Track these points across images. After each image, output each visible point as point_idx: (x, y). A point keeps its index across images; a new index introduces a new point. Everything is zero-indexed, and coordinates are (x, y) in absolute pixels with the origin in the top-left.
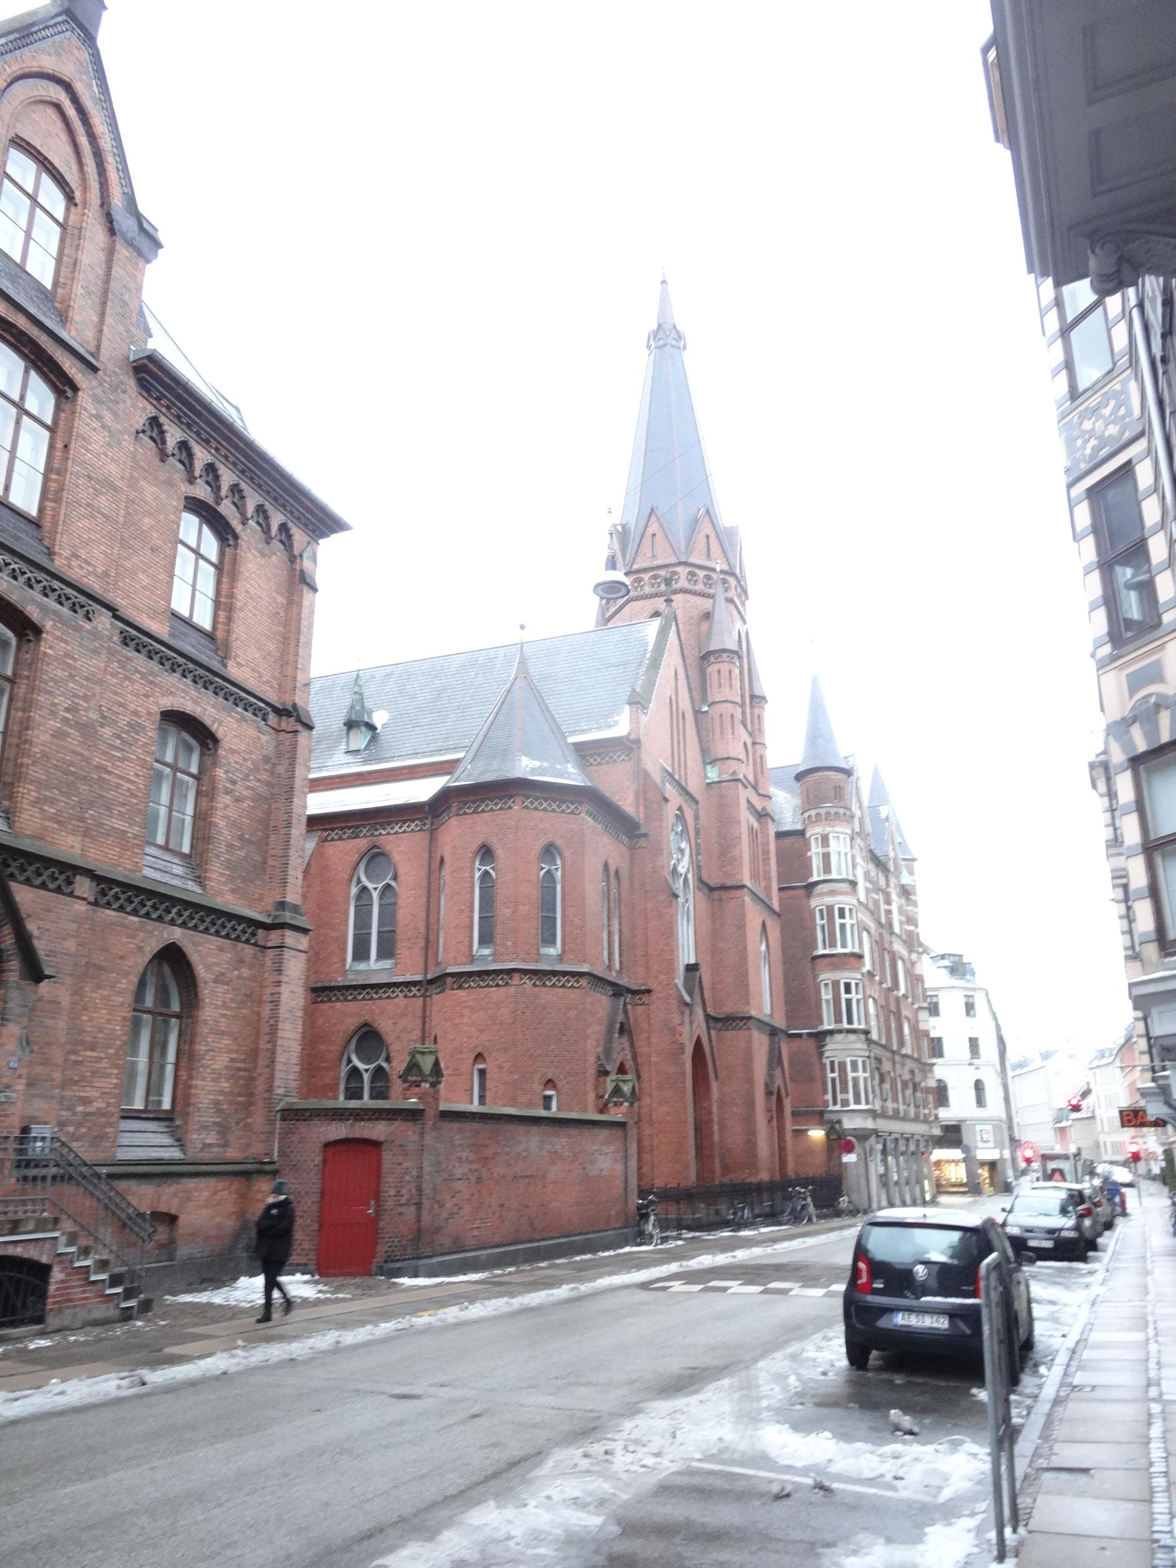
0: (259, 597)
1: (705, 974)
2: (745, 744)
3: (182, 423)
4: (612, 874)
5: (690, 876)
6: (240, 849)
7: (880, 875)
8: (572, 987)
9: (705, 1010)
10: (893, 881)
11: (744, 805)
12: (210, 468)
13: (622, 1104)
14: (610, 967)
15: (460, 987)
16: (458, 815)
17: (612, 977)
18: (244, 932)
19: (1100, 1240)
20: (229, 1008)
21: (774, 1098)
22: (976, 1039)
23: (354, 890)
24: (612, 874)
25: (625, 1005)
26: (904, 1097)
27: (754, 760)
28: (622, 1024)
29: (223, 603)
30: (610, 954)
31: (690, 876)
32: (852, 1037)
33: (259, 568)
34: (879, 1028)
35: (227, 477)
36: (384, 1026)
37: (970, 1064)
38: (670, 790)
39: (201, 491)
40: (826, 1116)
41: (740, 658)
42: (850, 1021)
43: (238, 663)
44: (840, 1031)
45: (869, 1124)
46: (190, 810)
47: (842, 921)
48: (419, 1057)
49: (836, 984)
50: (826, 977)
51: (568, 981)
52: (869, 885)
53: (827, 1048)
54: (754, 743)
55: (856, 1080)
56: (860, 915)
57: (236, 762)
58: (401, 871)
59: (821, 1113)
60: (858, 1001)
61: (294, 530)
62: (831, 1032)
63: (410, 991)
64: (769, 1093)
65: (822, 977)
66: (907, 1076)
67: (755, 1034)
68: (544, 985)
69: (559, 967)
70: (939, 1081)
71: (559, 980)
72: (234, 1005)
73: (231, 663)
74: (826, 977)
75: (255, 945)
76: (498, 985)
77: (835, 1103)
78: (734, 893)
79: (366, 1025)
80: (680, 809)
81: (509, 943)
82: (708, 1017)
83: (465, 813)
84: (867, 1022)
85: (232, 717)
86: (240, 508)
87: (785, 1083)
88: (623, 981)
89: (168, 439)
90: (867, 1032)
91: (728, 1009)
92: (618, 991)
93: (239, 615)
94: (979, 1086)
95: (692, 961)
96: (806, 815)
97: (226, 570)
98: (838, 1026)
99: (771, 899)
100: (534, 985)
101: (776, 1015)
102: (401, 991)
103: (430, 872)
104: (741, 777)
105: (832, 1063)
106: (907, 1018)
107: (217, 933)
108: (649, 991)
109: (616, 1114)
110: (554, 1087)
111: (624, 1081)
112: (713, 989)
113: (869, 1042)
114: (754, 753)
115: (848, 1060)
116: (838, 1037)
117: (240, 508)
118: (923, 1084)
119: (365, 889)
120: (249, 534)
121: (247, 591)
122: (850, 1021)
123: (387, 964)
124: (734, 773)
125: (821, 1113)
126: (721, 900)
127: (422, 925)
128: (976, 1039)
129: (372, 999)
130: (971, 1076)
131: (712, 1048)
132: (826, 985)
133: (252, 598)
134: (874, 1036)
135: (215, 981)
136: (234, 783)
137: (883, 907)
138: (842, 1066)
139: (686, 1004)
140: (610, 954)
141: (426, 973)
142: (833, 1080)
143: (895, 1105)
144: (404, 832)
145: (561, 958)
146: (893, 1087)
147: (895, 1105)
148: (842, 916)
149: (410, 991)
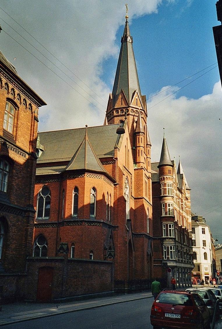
0: (24, 124)
1: (132, 222)
2: (145, 158)
3: (13, 84)
4: (109, 195)
5: (129, 195)
6: (19, 191)
7: (180, 193)
8: (98, 226)
9: (132, 232)
10: (183, 195)
11: (144, 175)
12: (13, 89)
13: (111, 258)
14: (108, 220)
15: (68, 225)
16: (69, 178)
17: (108, 223)
18: (15, 211)
19: (37, 148)
20: (16, 233)
21: (149, 257)
22: (205, 241)
23: (38, 197)
24: (109, 195)
25: (112, 230)
26: (184, 257)
27: (147, 162)
28: (111, 236)
29: (16, 127)
30: (108, 217)
31: (129, 195)
32: (171, 240)
33: (24, 115)
34: (178, 237)
35: (17, 91)
36: (46, 235)
37: (203, 248)
38: (125, 172)
39: (11, 96)
40: (163, 262)
41: (144, 134)
42: (170, 236)
43: (19, 142)
44: (167, 238)
45: (175, 264)
46: (6, 181)
47: (169, 208)
48: (63, 245)
49: (167, 225)
50: (164, 223)
51: (97, 224)
52: (177, 197)
53: (164, 242)
54: (147, 158)
55: (171, 252)
56: (174, 206)
57: (18, 168)
58: (52, 192)
59: (161, 261)
60: (173, 230)
61: (33, 105)
62: (165, 238)
63: (54, 226)
64: (148, 255)
65: (163, 223)
66: (185, 251)
67: (145, 239)
68: (91, 225)
69: (95, 220)
70: (194, 252)
71: (95, 224)
72: (17, 232)
73: (17, 142)
74: (164, 223)
75: (22, 216)
76: (78, 225)
77: (166, 258)
78: (141, 200)
79: (41, 234)
80: (127, 176)
81: (82, 214)
82: (132, 233)
83: (71, 178)
84: (175, 236)
85: (17, 156)
86: (20, 99)
87: (152, 252)
88: (111, 224)
89: (3, 83)
90: (175, 239)
91: (138, 232)
92: (110, 227)
93: (19, 129)
94: (205, 254)
95: (129, 218)
96: (160, 178)
97: (17, 117)
98: (167, 237)
99: (150, 201)
100: (88, 225)
101: (150, 234)
102: (51, 226)
103: (60, 193)
104: (144, 168)
105: (165, 247)
106: (186, 235)
107: (13, 213)
108: (118, 227)
109: (109, 260)
110: (93, 253)
111: (112, 252)
112: (134, 226)
113: (175, 241)
114: (147, 161)
115: (169, 246)
116: (167, 240)
117: (20, 99)
118: (189, 253)
119: (42, 197)
120: (22, 107)
121: (21, 122)
122: (170, 236)
123: (47, 218)
124: (142, 167)
125: (161, 261)
126: (137, 201)
127: (57, 207)
128: (205, 241)
129: (43, 227)
130: (203, 251)
131: (133, 242)
132: (164, 225)
133: (22, 124)
134: (177, 240)
135: (12, 226)
136: (17, 173)
137: (180, 203)
138: (168, 248)
139: (128, 231)
140: (108, 217)
141: (58, 221)
142: (165, 251)
143: (182, 259)
144: (53, 182)
145: (95, 218)
146: (181, 254)
147: (182, 259)
148: (169, 206)
149: (54, 226)
